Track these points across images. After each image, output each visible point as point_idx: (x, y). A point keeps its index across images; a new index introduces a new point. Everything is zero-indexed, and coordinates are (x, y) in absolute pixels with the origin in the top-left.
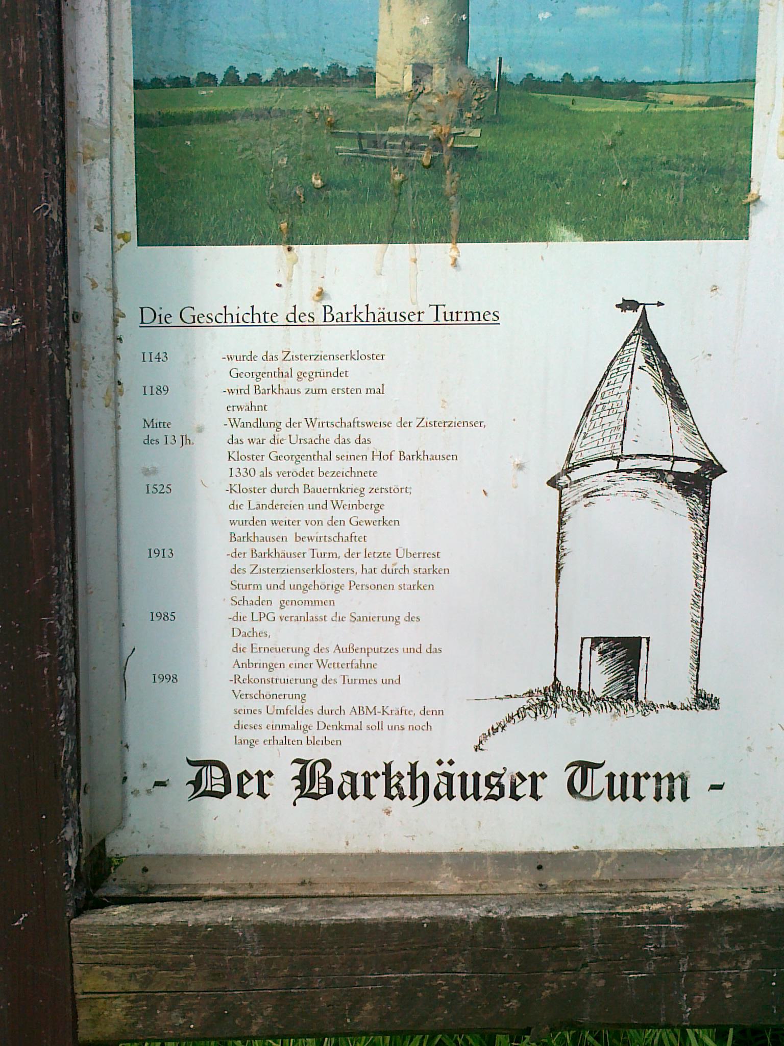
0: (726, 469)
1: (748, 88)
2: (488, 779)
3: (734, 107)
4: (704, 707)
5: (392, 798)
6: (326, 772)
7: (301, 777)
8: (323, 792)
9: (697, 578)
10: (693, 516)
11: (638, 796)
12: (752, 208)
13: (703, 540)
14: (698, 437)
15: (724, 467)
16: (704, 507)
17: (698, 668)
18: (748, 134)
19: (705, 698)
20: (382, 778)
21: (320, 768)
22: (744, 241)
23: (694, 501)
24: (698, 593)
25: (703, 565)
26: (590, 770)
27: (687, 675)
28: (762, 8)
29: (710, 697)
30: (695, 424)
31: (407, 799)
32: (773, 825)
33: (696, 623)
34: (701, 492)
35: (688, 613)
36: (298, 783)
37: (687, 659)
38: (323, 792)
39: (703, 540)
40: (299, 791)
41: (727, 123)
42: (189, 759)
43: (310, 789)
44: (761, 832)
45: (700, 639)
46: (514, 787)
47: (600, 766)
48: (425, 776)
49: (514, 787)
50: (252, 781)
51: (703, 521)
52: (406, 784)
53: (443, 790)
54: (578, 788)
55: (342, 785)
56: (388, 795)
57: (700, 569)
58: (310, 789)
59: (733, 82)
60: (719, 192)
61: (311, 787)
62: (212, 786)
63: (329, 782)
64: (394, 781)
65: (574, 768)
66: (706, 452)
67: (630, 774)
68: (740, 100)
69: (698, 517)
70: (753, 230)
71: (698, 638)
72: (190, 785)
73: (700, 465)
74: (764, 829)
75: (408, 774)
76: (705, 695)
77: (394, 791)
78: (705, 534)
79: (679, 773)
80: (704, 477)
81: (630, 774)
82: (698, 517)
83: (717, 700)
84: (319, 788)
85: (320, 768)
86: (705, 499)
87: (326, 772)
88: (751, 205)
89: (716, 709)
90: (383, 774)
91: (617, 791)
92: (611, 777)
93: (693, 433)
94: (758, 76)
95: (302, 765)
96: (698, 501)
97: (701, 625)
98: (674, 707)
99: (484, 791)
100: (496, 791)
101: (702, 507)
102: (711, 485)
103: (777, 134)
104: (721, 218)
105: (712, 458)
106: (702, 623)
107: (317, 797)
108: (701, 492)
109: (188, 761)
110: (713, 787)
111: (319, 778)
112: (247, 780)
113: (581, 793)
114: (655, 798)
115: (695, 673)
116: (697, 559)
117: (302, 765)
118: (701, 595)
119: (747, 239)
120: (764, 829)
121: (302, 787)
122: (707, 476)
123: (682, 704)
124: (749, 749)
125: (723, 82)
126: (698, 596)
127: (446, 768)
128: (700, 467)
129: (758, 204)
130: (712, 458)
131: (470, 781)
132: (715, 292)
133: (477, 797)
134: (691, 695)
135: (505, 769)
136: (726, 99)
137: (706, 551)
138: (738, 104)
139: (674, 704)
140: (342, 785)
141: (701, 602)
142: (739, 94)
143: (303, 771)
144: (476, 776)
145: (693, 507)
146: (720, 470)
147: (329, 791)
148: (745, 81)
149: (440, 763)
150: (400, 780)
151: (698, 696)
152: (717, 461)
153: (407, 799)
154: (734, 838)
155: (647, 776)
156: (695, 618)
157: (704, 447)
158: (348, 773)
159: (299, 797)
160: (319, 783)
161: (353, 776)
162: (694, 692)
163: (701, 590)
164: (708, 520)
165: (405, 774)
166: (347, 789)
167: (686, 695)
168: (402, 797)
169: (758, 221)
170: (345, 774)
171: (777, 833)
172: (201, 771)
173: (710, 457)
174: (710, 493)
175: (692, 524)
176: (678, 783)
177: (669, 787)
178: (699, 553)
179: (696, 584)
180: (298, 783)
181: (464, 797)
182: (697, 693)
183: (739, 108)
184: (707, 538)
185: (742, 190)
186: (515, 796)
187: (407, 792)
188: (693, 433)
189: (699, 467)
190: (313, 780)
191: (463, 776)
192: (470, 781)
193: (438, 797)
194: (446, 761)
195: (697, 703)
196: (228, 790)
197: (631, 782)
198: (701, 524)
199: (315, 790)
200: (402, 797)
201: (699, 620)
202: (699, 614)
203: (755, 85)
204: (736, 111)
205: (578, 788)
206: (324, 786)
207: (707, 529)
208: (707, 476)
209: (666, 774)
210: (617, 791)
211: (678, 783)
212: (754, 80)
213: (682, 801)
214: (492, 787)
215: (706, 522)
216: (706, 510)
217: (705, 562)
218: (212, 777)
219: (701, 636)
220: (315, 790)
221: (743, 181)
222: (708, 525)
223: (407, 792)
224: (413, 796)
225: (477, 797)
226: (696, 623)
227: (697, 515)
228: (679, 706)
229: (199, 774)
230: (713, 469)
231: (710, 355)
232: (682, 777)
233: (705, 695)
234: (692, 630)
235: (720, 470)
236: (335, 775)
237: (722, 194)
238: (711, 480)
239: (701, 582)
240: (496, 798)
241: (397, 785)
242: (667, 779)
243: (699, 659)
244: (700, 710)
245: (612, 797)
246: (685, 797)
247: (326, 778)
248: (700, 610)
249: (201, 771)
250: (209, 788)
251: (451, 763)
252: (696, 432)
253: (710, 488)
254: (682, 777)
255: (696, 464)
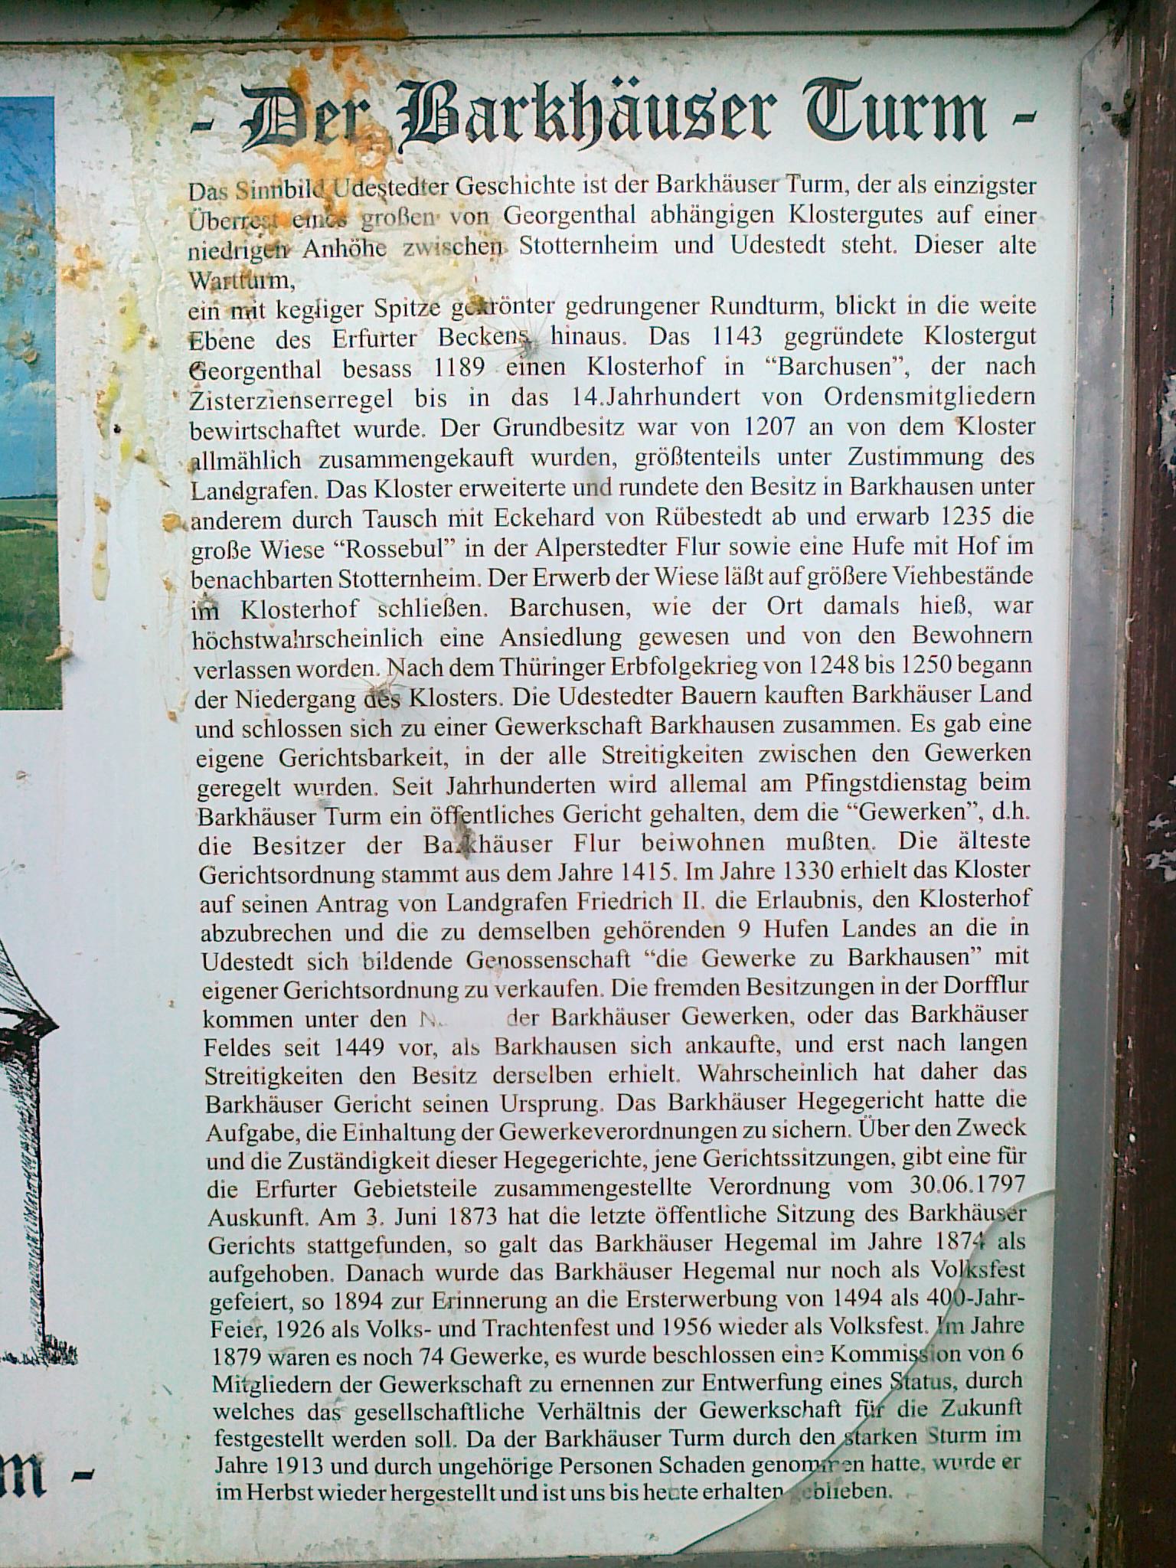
0: (58, 1024)
1: (48, 506)
2: (689, 105)
3: (31, 530)
4: (55, 1360)
5: (547, 137)
6: (448, 101)
7: (411, 109)
8: (443, 131)
9: (29, 1177)
10: (16, 1089)
11: (912, 132)
12: (64, 667)
13: (32, 1122)
14: (14, 978)
15: (55, 1020)
16: (31, 1077)
17: (43, 1305)
18: (52, 567)
19: (55, 1348)
20: (532, 107)
21: (440, 94)
22: (57, 711)
23: (17, 1068)
24: (33, 1199)
25: (36, 1159)
26: (839, 92)
27: (27, 1314)
28: (59, 403)
29: (63, 1345)
30: (9, 961)
31: (570, 139)
32: (171, 1532)
33: (34, 1240)
34: (25, 1057)
35: (20, 1226)
36: (406, 117)
37: (25, 1292)
38: (443, 131)
39: (32, 1122)
40: (407, 130)
41: (23, 552)
42: (245, 86)
43: (424, 127)
44: (155, 1543)
45: (41, 1264)
46: (728, 119)
47: (855, 85)
48: (596, 102)
49: (728, 119)
50: (337, 117)
51: (31, 1097)
52: (567, 115)
53: (623, 123)
54: (823, 118)
55: (472, 118)
56: (541, 132)
57: (33, 1165)
58: (424, 127)
59: (27, 497)
60: (17, 647)
61: (425, 125)
62: (278, 127)
63: (453, 114)
64: (550, 111)
65: (817, 88)
66: (28, 999)
67: (899, 97)
68: (38, 522)
69: (24, 1091)
70: (68, 695)
71: (39, 1262)
72: (246, 127)
73: (20, 1017)
74: (157, 1538)
75: (571, 99)
76: (56, 1343)
77: (550, 127)
78: (35, 1114)
79: (28, 1456)
80: (28, 1035)
81: (899, 97)
82: (24, 1091)
83: (72, 1351)
84: (437, 126)
85: (440, 94)
86: (31, 1066)
87: (448, 101)
88: (63, 663)
89: (73, 1364)
90: (533, 100)
91: (881, 124)
92: (871, 101)
93: (8, 974)
94: (59, 493)
95: (411, 92)
96: (22, 1069)
97: (42, 1244)
98: (14, 1361)
99: (683, 124)
100: (701, 124)
101: (28, 1077)
102: (38, 1045)
103: (91, 566)
104: (22, 681)
105: (37, 1009)
106: (42, 1240)
107: (434, 138)
108: (25, 1057)
109: (243, 89)
110: (78, 1476)
111: (438, 109)
112: (331, 115)
113: (829, 128)
114: (936, 135)
115: (39, 1312)
116: (27, 1150)
117: (411, 92)
118: (37, 1201)
119: (60, 708)
120: (157, 1538)
121: (411, 124)
122: (32, 1034)
123: (25, 1356)
124: (125, 1420)
125: (14, 498)
126: (33, 1203)
127: (626, 89)
128: (20, 1021)
129: (72, 661)
130: (37, 1009)
131: (663, 108)
132: (22, 781)
133: (673, 132)
134: (37, 1344)
135: (714, 90)
136: (20, 520)
137: (39, 1139)
138: (36, 526)
139: (14, 1355)
140: (472, 118)
141: (38, 1212)
142: (38, 514)
143: (414, 100)
144: (672, 101)
145: (15, 1076)
146: (49, 1026)
147: (453, 128)
148: (44, 496)
149: (617, 82)
150: (559, 109)
151: (46, 1345)
152: (43, 1012)
153: (570, 139)
154: (114, 1551)
155: (923, 101)
156: (32, 1234)
157: (25, 993)
158: (482, 101)
159: (408, 139)
160: (437, 117)
161: (489, 104)
162: (41, 1338)
163: (37, 1195)
164: (38, 1095)
165: (565, 99)
166: (479, 125)
167: (30, 1344)
168: (562, 135)
169: (71, 682)
170: (476, 102)
171: (176, 1544)
172: (262, 104)
173: (34, 1007)
174: (38, 1057)
175: (16, 1100)
176: (28, 1470)
177: (16, 1475)
178: (30, 1143)
179: (29, 1185)
180: (406, 117)
181: (655, 132)
182: (44, 1340)
183: (37, 532)
184: (38, 1121)
185: (50, 641)
186: (730, 132)
187: (569, 128)
188: (8, 974)
189: (20, 1021)
190: (428, 113)
191: (653, 100)
192: (663, 108)
193: (616, 134)
194: (626, 79)
195: (46, 1355)
196: (302, 133)
197: (900, 110)
198: (28, 1102)
199: (431, 128)
200: (562, 135)
201: (38, 1236)
202: (37, 1228)
203: (56, 502)
204: (34, 536)
205: (823, 118)
206: (446, 121)
207: (38, 1107)
208: (32, 1034)
209: (10, 1457)
210: (881, 124)
211: (28, 1470)
212: (55, 496)
213: (34, 1496)
214: (695, 118)
215: (35, 1097)
216: (34, 1081)
217: (38, 1154)
218: (278, 114)
219: (42, 1260)
220: (431, 128)
221: (49, 630)
222: (38, 1101)
223: (569, 128)
224: (579, 135)
225: (673, 132)
226: (34, 1240)
227: (21, 1088)
228: (21, 1359)
229: (261, 106)
230: (39, 1024)
231: (23, 866)
232: (33, 1460)
233: (56, 1343)
234: (30, 1250)
235: (49, 1026)
236: (462, 104)
237: (21, 648)
238: (38, 1040)
239: (35, 1183)
240: (702, 135)
241: (555, 117)
242: (11, 1464)
243: (42, 1291)
244: (51, 1365)
245: (873, 134)
246: (39, 1490)
247: (448, 109)
248: (37, 1222)
249: (262, 104)
250: (273, 131)
251: (634, 81)
252: (12, 973)
253: (38, 1050)
254: (33, 1460)
255: (15, 1017)
